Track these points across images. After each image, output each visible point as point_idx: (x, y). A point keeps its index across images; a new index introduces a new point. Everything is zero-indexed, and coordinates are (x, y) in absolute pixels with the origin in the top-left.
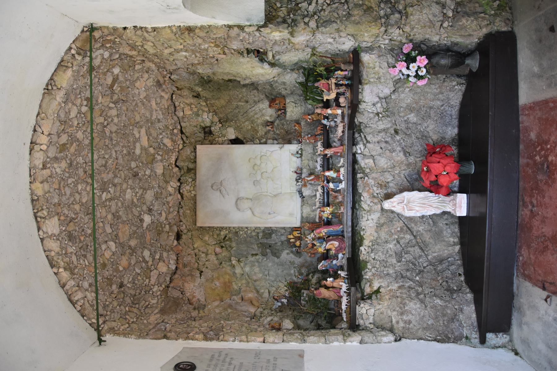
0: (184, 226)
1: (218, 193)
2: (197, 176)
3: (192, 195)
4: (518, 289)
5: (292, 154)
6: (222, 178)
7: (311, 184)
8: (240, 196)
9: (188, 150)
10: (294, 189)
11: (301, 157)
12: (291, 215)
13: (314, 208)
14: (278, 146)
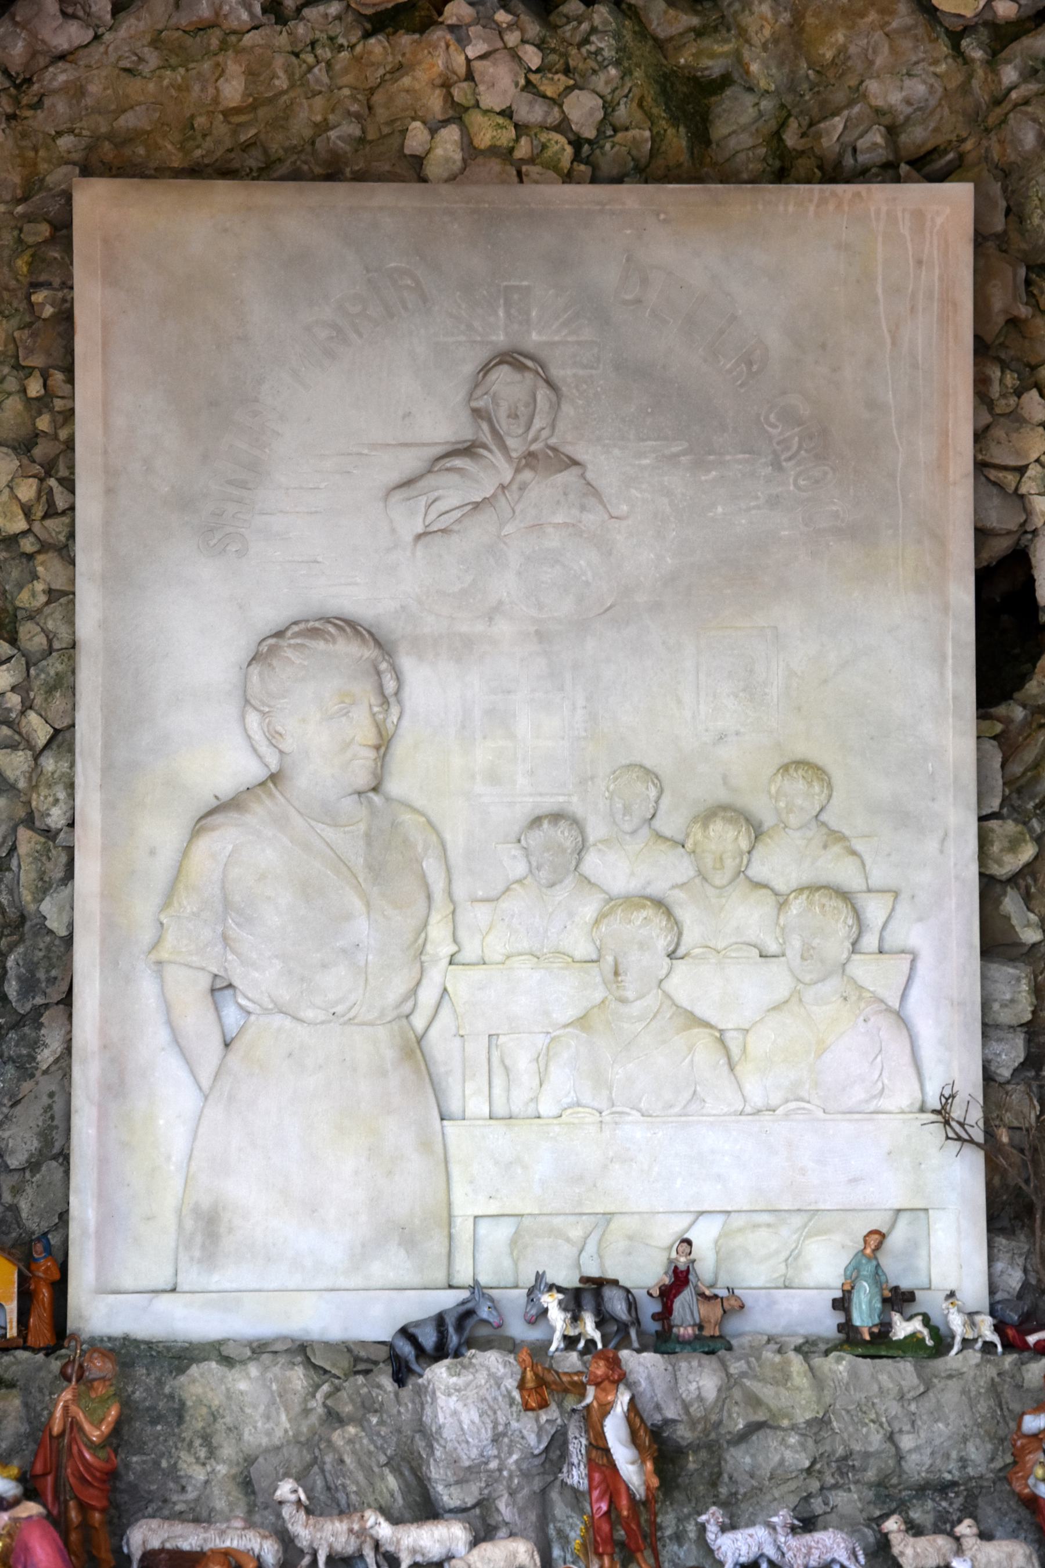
0: (74, 34)
1: (441, 424)
2: (631, 196)
3: (417, 137)
4: (448, 470)
5: (877, 1239)
6: (604, 465)
7: (558, 1444)
8: (407, 663)
9: (918, 89)
10: (488, 1260)
11: (849, 1337)
12: (208, 1230)
13: (286, 1489)
14: (970, 1084)
